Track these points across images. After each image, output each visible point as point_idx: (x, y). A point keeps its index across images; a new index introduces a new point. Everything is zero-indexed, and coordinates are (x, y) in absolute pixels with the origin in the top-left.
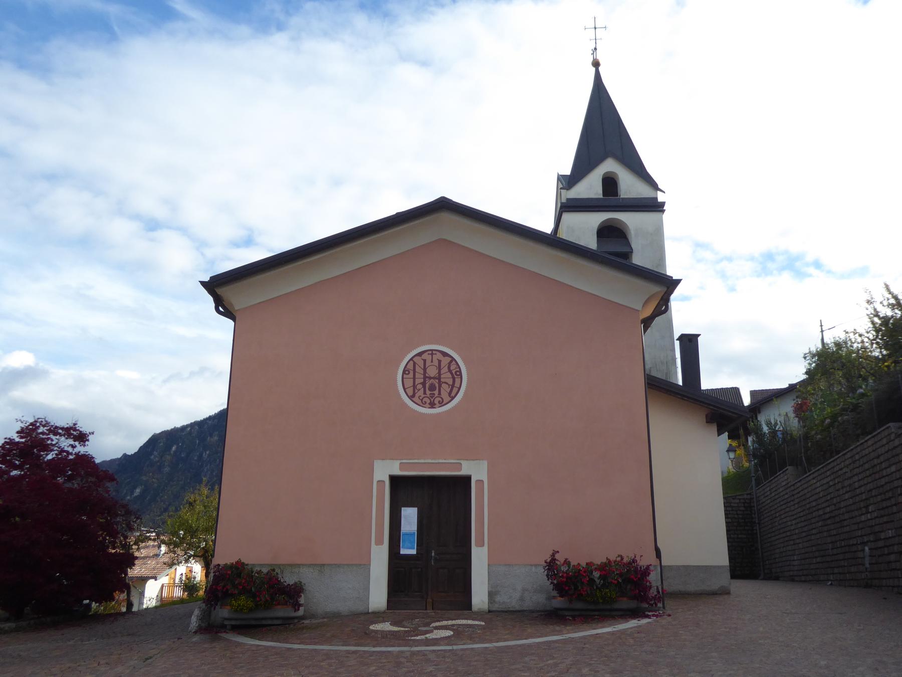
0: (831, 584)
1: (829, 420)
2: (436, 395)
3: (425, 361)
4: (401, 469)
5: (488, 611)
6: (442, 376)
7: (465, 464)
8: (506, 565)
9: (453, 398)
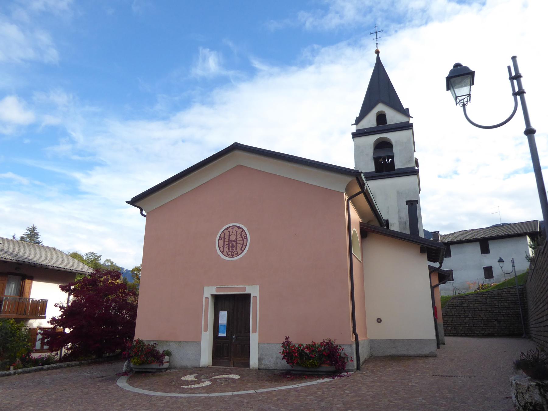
2: (235, 250)
3: (229, 232)
4: (216, 291)
5: (258, 369)
8: (268, 343)
9: (243, 251)
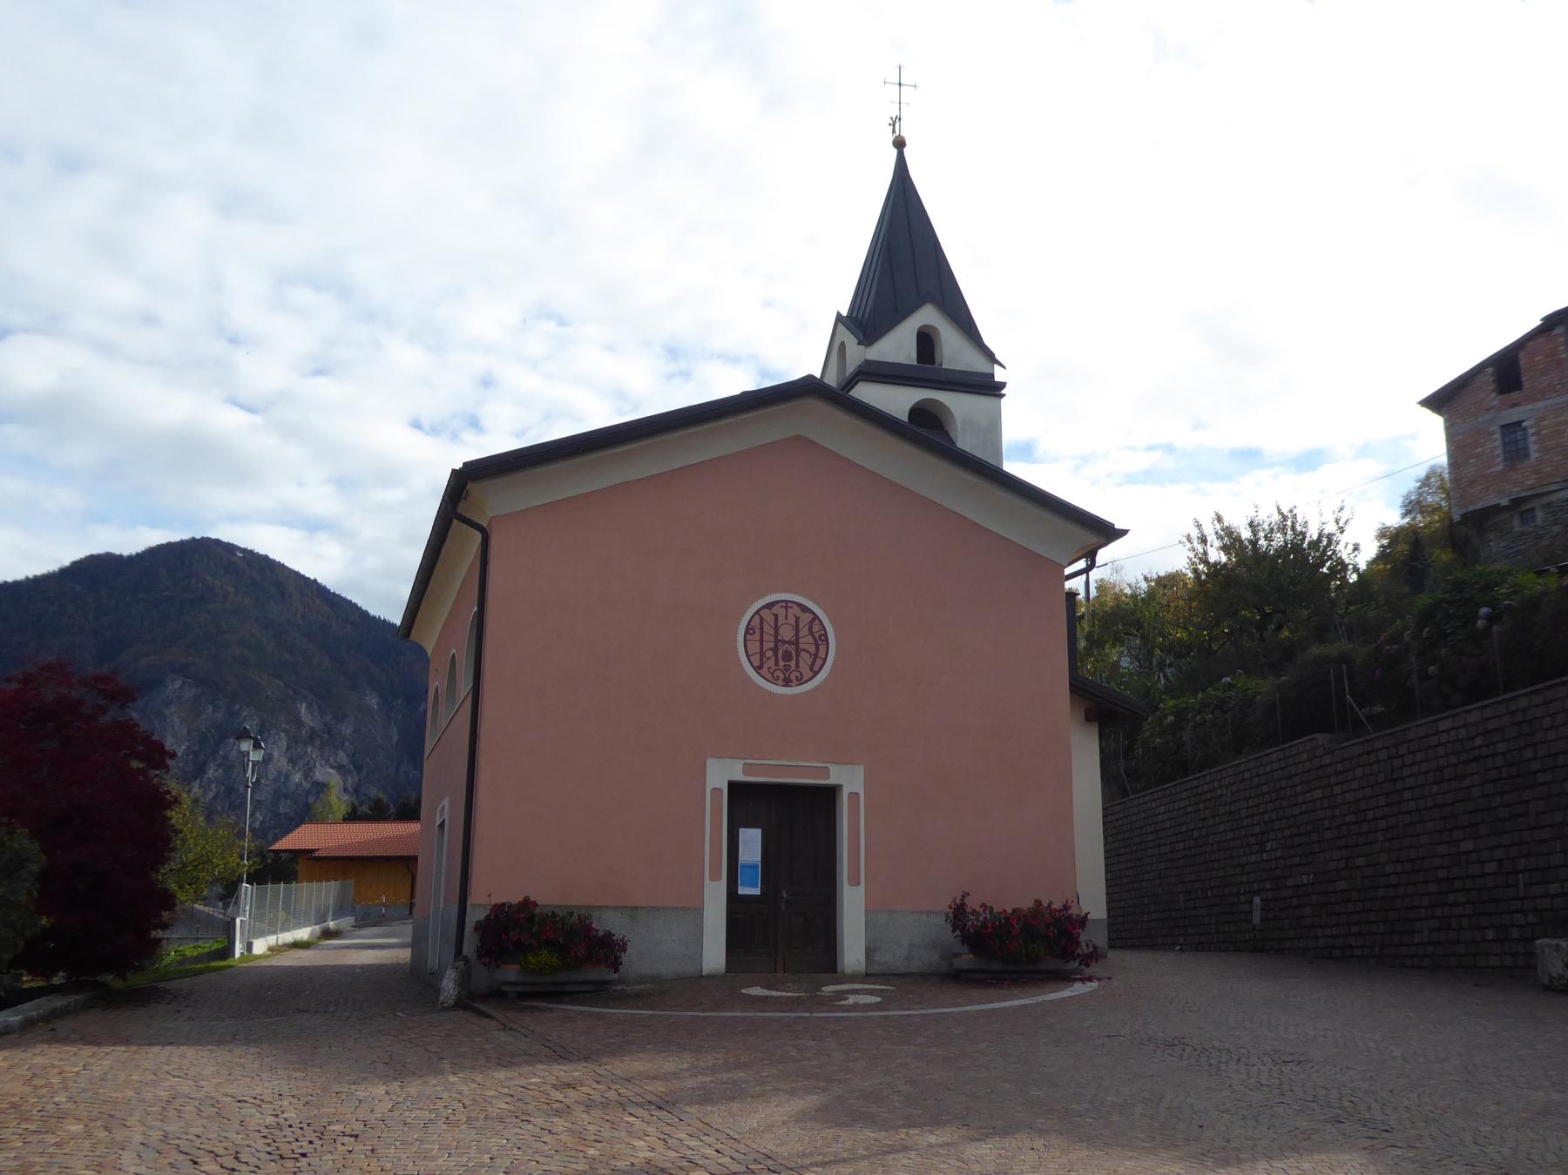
0: (1180, 950)
1: (1173, 718)
2: (793, 668)
3: (776, 616)
4: (745, 773)
6: (801, 641)
7: (833, 768)
9: (816, 674)
